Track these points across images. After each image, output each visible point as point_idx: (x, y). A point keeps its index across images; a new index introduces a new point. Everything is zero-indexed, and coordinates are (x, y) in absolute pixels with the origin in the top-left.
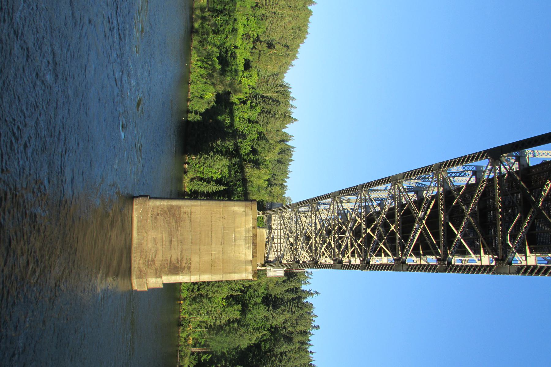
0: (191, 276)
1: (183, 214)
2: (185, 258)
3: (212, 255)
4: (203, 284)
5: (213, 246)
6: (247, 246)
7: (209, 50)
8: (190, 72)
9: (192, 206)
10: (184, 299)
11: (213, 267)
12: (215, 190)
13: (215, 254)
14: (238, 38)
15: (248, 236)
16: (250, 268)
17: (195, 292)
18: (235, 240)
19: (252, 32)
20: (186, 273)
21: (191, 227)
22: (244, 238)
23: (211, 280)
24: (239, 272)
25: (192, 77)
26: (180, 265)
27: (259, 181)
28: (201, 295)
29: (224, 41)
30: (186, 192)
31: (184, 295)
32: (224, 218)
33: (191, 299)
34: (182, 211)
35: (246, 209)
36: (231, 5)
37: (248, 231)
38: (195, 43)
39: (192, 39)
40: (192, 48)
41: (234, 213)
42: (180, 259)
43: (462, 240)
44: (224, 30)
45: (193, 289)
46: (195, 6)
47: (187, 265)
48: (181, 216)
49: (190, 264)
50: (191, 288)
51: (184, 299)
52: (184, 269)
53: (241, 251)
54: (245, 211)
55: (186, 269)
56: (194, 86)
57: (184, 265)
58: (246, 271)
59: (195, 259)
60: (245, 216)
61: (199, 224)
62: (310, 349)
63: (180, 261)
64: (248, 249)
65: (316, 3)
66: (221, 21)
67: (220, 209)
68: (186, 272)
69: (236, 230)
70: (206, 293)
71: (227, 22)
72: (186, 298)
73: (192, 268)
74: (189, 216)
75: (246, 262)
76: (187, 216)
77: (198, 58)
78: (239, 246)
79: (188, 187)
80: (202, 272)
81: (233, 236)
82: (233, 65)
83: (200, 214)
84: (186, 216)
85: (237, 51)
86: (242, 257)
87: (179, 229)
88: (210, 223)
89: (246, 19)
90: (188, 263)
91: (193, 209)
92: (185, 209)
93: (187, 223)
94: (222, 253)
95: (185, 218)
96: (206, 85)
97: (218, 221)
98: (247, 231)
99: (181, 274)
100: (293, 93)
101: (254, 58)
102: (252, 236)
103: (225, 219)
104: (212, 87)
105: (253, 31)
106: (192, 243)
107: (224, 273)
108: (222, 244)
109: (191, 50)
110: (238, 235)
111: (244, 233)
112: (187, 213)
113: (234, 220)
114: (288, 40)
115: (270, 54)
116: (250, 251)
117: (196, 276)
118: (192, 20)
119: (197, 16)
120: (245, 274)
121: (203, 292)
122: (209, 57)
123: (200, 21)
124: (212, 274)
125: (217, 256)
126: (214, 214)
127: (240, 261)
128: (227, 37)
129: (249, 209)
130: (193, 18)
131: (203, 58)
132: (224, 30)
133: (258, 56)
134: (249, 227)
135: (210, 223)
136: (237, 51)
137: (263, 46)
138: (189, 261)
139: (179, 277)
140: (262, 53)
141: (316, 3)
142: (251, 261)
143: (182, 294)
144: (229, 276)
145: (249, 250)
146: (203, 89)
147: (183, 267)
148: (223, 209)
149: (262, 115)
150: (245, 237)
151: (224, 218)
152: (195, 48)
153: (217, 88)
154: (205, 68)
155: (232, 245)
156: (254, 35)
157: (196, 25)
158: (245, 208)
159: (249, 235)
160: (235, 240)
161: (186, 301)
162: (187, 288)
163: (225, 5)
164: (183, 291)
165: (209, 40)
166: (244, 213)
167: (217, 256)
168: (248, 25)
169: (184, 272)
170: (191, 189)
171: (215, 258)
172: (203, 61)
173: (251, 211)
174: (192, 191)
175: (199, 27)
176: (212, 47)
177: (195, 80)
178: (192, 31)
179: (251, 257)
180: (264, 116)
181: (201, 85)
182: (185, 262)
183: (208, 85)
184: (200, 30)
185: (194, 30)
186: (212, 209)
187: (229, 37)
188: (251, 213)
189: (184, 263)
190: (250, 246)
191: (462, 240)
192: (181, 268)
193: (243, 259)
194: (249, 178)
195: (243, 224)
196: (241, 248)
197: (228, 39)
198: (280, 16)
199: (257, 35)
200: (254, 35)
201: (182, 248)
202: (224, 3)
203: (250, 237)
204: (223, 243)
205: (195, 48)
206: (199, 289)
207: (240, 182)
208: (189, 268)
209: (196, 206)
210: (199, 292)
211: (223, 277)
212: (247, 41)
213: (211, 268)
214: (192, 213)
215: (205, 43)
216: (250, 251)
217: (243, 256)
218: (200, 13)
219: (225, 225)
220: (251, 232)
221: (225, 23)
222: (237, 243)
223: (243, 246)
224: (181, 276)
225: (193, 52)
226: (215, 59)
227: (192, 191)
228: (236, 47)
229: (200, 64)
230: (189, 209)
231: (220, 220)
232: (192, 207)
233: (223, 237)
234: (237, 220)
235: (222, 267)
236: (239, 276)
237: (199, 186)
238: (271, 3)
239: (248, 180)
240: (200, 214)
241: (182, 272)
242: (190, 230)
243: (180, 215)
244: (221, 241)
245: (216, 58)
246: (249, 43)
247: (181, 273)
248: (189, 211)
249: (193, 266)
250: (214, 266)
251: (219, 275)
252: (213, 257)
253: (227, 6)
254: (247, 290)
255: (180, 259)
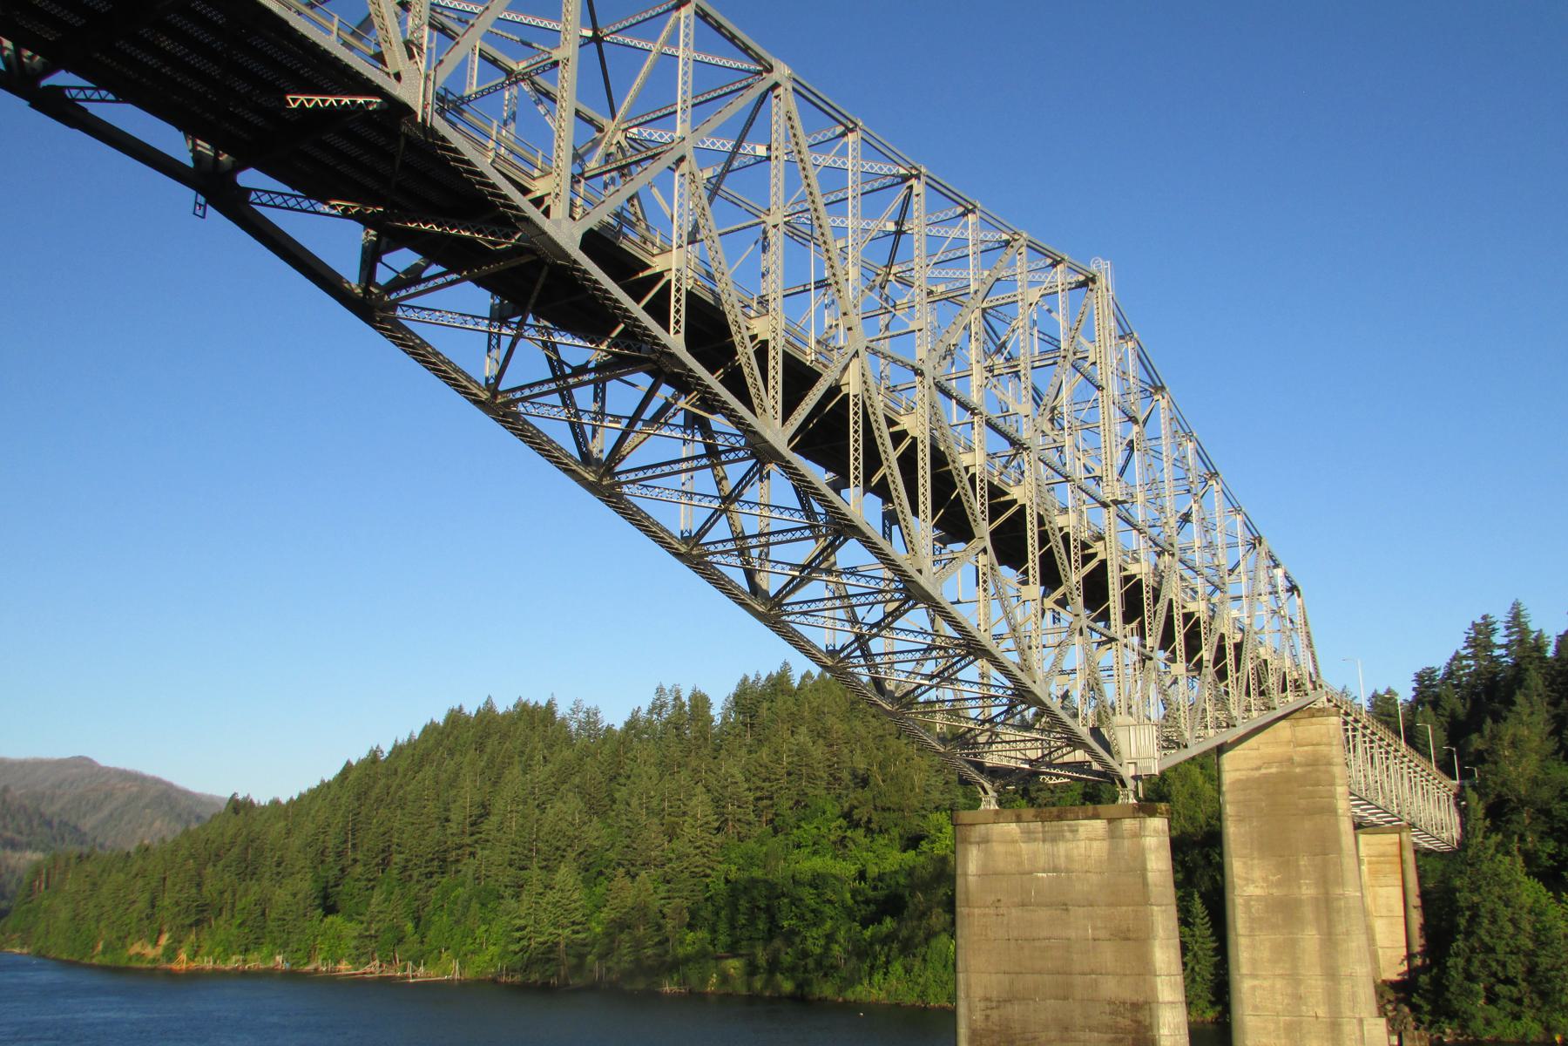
0: (1160, 1000)
1: (990, 1023)
2: (1107, 1019)
3: (1096, 937)
4: (1489, 966)
5: (1072, 934)
6: (1068, 835)
7: (846, 951)
8: (898, 1005)
9: (968, 996)
10: (1549, 1029)
11: (1131, 935)
12: (1208, 929)
13: (1094, 928)
14: (833, 871)
15: (1044, 832)
16: (1128, 824)
17: (1520, 991)
18: (1055, 869)
19: (833, 832)
20: (1151, 1016)
21: (1024, 999)
22: (1048, 846)
23: (1177, 941)
24: (1140, 856)
25: (910, 999)
26: (1130, 1032)
27: (1207, 794)
28: (1531, 971)
29: (840, 908)
30: (1217, 1019)
31: (1535, 1031)
32: (997, 904)
33: (1547, 1008)
34: (983, 1026)
35: (972, 840)
36: (755, 893)
37: (1029, 832)
38: (827, 990)
39: (820, 999)
40: (840, 1000)
41: (984, 874)
42: (1113, 1036)
43: (613, 335)
44: (813, 911)
45: (1511, 999)
46: (743, 991)
47: (1128, 1014)
48: (996, 1028)
49: (1124, 1003)
50: (1510, 1007)
51: (1549, 1029)
52: (1138, 1022)
53: (1083, 851)
54: (978, 843)
55: (1140, 1017)
56: (931, 991)
57: (1127, 1022)
58: (1138, 835)
59: (1111, 988)
60: (989, 844)
61: (1014, 976)
62: (532, 703)
63: (1116, 1033)
64: (1077, 831)
65: (786, 664)
66: (792, 919)
67: (973, 915)
68: (1148, 1017)
69: (1027, 867)
70: (1522, 959)
71: (796, 901)
72: (1543, 1023)
73: (1134, 999)
74: (994, 1004)
75: (1113, 835)
76: (995, 1011)
77: (866, 982)
78: (1068, 858)
79: (1204, 1012)
80: (1145, 969)
81: (1044, 875)
82: (898, 883)
83: (990, 973)
84: (995, 1015)
85: (873, 871)
86: (1099, 848)
87: (1029, 1035)
88: (1013, 942)
89: (797, 851)
90: (1122, 1009)
91: (978, 992)
92: (978, 1016)
93: (1015, 1011)
94: (1090, 908)
95: (1000, 1016)
96: (928, 958)
97: (1005, 919)
98: (1029, 836)
99: (1155, 1032)
100: (358, 754)
101: (896, 825)
102: (1043, 822)
103: (999, 901)
104: (933, 943)
105: (830, 830)
106: (1065, 998)
107: (1146, 902)
108: (1067, 910)
109: (846, 1002)
110: (1041, 862)
111: (1033, 846)
112: (989, 1012)
113: (1003, 874)
114: (880, 732)
115: (884, 781)
116: (1082, 825)
117: (1159, 987)
118: (779, 999)
119: (765, 987)
120: (1148, 839)
121: (1516, 968)
122: (861, 952)
123: (779, 977)
124: (1149, 938)
125: (1099, 924)
126: (989, 932)
127: (1112, 852)
128: (830, 902)
129: (972, 834)
130: (770, 997)
131: (866, 967)
132: (813, 911)
133: (886, 815)
134: (1018, 830)
135: (1013, 942)
136: (873, 871)
137: (861, 799)
138: (1116, 1006)
139: (1163, 1038)
140: (878, 803)
141: (786, 664)
142: (1110, 821)
143: (1532, 1038)
144: (1156, 885)
145: (1081, 829)
146: (939, 966)
147: (1134, 1025)
148: (974, 907)
149: (1033, 795)
150: (1044, 841)
151: (997, 904)
152: (841, 990)
153: (938, 928)
154: (888, 962)
155: (1069, 878)
156: (840, 827)
157: (788, 986)
158: (970, 843)
159: (1041, 829)
160: (1055, 869)
161: (1553, 1023)
162: (1509, 1019)
163: (759, 908)
164: (1521, 1033)
165: (818, 951)
166: (983, 846)
167: (1099, 924)
168: (814, 844)
169: (1147, 1024)
170: (1210, 1002)
171: (1105, 928)
172: (872, 967)
173: (977, 827)
174: (1213, 999)
175: (793, 978)
176: (837, 942)
177: (918, 989)
178: (801, 999)
179: (1099, 821)
180: (1036, 787)
181: (928, 973)
182: (1119, 1019)
183: (929, 952)
184: (800, 976)
185: (799, 992)
186: (976, 938)
187: (829, 895)
188: (983, 827)
189: (1125, 1022)
190: (1068, 825)
191: (613, 335)
192: (1137, 1032)
193: (1105, 845)
194: (1201, 827)
195: (1011, 848)
196: (1075, 851)
197: (834, 898)
198: (795, 759)
199: (839, 817)
200: (840, 827)
201: (1083, 1028)
202: (753, 912)
203: (1044, 827)
204: (1065, 907)
205: (841, 990)
206: (1509, 981)
207: (1211, 852)
208: (1136, 1007)
209: (968, 986)
210: (1520, 981)
211: (1161, 905)
212: (850, 845)
213: (1134, 939)
214: (988, 996)
215: (826, 963)
216: (1082, 825)
217: (1096, 844)
218: (759, 976)
219: (1016, 900)
220: (1032, 825)
221: (797, 907)
222: (1062, 862)
223: (1071, 845)
224: (1162, 1032)
225: (850, 995)
226: (868, 933)
227: (1213, 999)
228: (862, 875)
229: (878, 977)
230: (978, 1004)
231: (1003, 915)
232: (972, 995)
233: (1050, 905)
234: (1001, 865)
235: (1130, 908)
236: (1153, 858)
237: (1198, 978)
238: (767, 784)
239: (1205, 829)
240: (990, 973)
241: (1150, 1028)
242: (1031, 1002)
243: (994, 1032)
244: (1058, 912)
245: (865, 932)
246: (853, 841)
247: (1152, 1030)
248: (982, 1005)
249: (1128, 995)
250: (1129, 930)
251: (1152, 915)
252: (1101, 934)
253: (758, 904)
254: (1560, 821)
255: (1113, 1036)
